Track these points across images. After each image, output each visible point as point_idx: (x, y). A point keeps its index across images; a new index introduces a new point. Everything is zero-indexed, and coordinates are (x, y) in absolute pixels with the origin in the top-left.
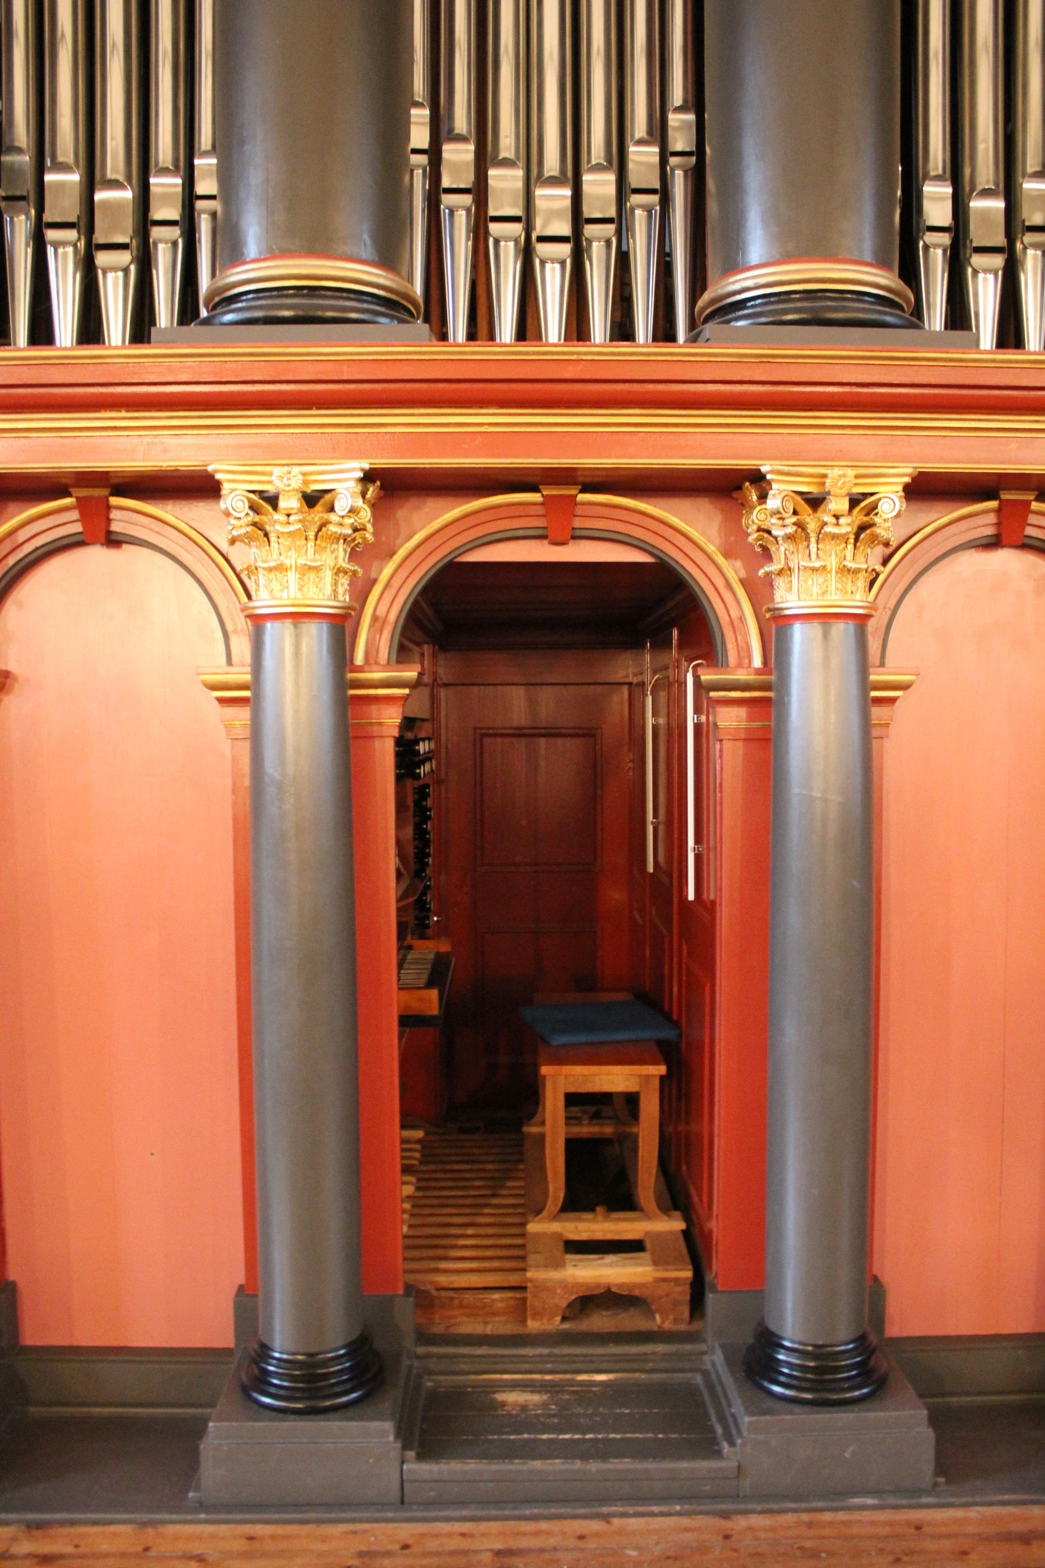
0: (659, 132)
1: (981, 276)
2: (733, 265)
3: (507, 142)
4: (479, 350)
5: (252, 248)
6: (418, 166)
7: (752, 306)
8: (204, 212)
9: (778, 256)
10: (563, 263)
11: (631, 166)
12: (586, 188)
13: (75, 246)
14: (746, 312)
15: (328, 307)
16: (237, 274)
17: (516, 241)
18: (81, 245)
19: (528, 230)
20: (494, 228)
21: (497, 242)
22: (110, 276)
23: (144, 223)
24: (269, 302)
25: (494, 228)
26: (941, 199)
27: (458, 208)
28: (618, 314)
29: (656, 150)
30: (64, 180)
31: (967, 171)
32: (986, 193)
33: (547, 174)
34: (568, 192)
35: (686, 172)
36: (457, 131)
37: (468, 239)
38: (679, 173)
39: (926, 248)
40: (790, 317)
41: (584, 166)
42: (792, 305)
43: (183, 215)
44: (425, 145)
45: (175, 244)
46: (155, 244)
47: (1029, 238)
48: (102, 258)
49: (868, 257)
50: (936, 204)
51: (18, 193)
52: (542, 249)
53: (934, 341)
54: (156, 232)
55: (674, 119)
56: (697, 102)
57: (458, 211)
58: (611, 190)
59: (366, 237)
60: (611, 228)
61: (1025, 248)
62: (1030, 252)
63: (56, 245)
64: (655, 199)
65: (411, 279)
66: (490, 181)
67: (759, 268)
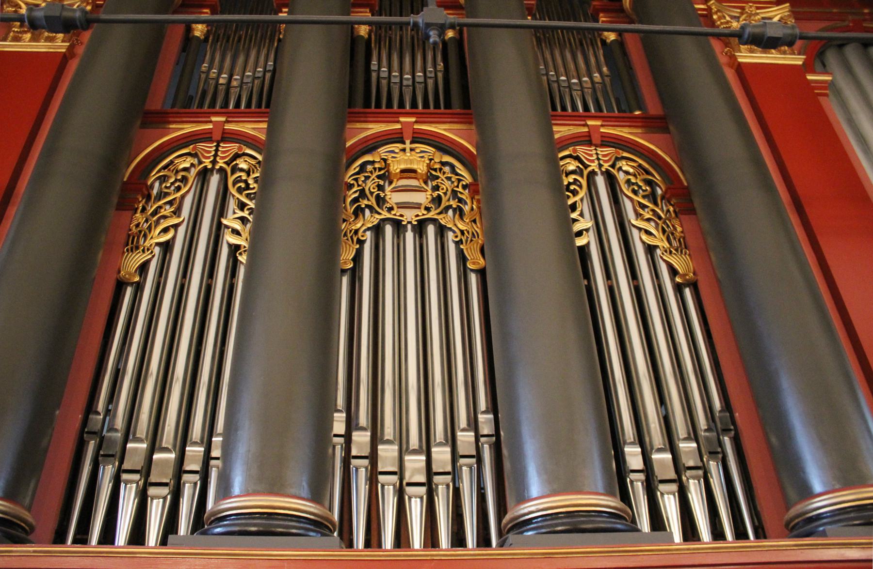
0: (473, 424)
1: (666, 496)
2: (523, 498)
3: (389, 431)
4: (373, 554)
5: (236, 489)
6: (338, 444)
7: (536, 522)
8: (215, 466)
9: (548, 492)
10: (421, 498)
11: (459, 443)
12: (434, 456)
13: (137, 483)
14: (532, 526)
15: (278, 525)
16: (227, 504)
17: (394, 485)
18: (141, 483)
19: (401, 479)
20: (381, 478)
21: (383, 486)
22: (155, 501)
23: (179, 470)
24: (243, 521)
25: (381, 478)
26: (634, 455)
27: (361, 467)
28: (455, 527)
29: (473, 434)
30: (138, 447)
31: (647, 439)
32: (659, 450)
33: (411, 448)
34: (424, 458)
35: (490, 446)
36: (361, 425)
37: (366, 484)
38: (486, 446)
39: (632, 482)
40: (560, 528)
41: (432, 443)
42: (560, 521)
43: (202, 468)
44: (343, 432)
45: (196, 484)
46: (184, 484)
47: (689, 473)
48: (152, 491)
49: (601, 491)
50: (633, 457)
51: (111, 453)
52: (410, 490)
53: (646, 539)
54: (186, 477)
55: (481, 418)
56: (494, 408)
57: (360, 469)
58: (448, 457)
59: (304, 484)
60: (449, 477)
61: (688, 479)
62: (691, 481)
63: (127, 482)
64: (474, 460)
65: (331, 509)
66: (379, 452)
67: (538, 500)
